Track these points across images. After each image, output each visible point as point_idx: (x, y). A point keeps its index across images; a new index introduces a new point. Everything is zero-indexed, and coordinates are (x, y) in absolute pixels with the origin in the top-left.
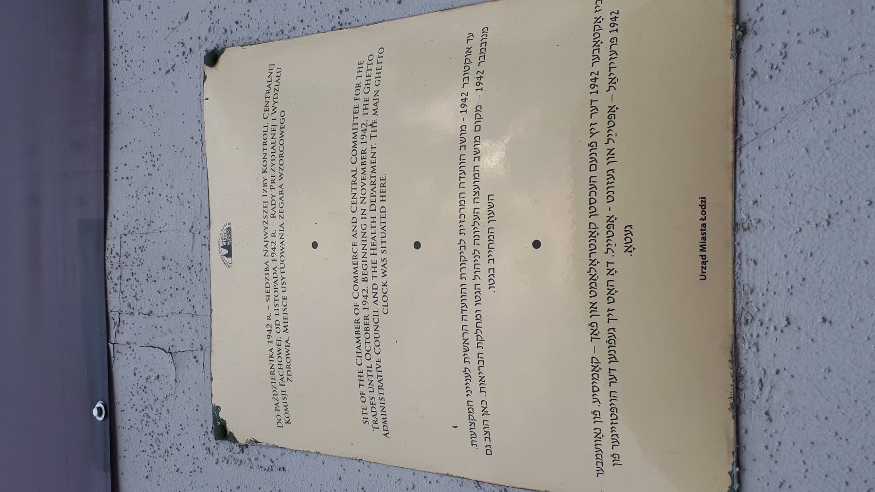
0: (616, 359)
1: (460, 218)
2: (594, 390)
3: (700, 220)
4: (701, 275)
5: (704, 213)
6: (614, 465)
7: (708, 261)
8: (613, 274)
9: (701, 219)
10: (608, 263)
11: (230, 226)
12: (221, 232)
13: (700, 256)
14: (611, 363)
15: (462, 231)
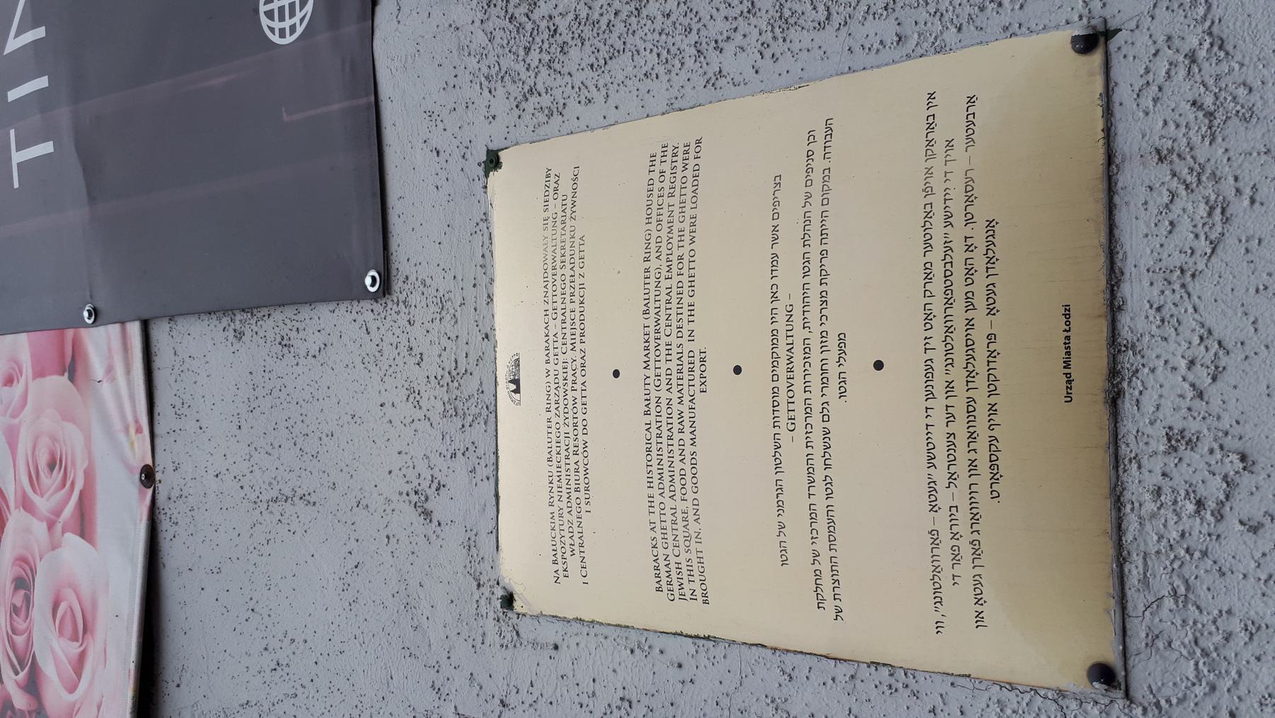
6: (977, 627)
9: (1065, 331)
10: (966, 238)
15: (809, 444)
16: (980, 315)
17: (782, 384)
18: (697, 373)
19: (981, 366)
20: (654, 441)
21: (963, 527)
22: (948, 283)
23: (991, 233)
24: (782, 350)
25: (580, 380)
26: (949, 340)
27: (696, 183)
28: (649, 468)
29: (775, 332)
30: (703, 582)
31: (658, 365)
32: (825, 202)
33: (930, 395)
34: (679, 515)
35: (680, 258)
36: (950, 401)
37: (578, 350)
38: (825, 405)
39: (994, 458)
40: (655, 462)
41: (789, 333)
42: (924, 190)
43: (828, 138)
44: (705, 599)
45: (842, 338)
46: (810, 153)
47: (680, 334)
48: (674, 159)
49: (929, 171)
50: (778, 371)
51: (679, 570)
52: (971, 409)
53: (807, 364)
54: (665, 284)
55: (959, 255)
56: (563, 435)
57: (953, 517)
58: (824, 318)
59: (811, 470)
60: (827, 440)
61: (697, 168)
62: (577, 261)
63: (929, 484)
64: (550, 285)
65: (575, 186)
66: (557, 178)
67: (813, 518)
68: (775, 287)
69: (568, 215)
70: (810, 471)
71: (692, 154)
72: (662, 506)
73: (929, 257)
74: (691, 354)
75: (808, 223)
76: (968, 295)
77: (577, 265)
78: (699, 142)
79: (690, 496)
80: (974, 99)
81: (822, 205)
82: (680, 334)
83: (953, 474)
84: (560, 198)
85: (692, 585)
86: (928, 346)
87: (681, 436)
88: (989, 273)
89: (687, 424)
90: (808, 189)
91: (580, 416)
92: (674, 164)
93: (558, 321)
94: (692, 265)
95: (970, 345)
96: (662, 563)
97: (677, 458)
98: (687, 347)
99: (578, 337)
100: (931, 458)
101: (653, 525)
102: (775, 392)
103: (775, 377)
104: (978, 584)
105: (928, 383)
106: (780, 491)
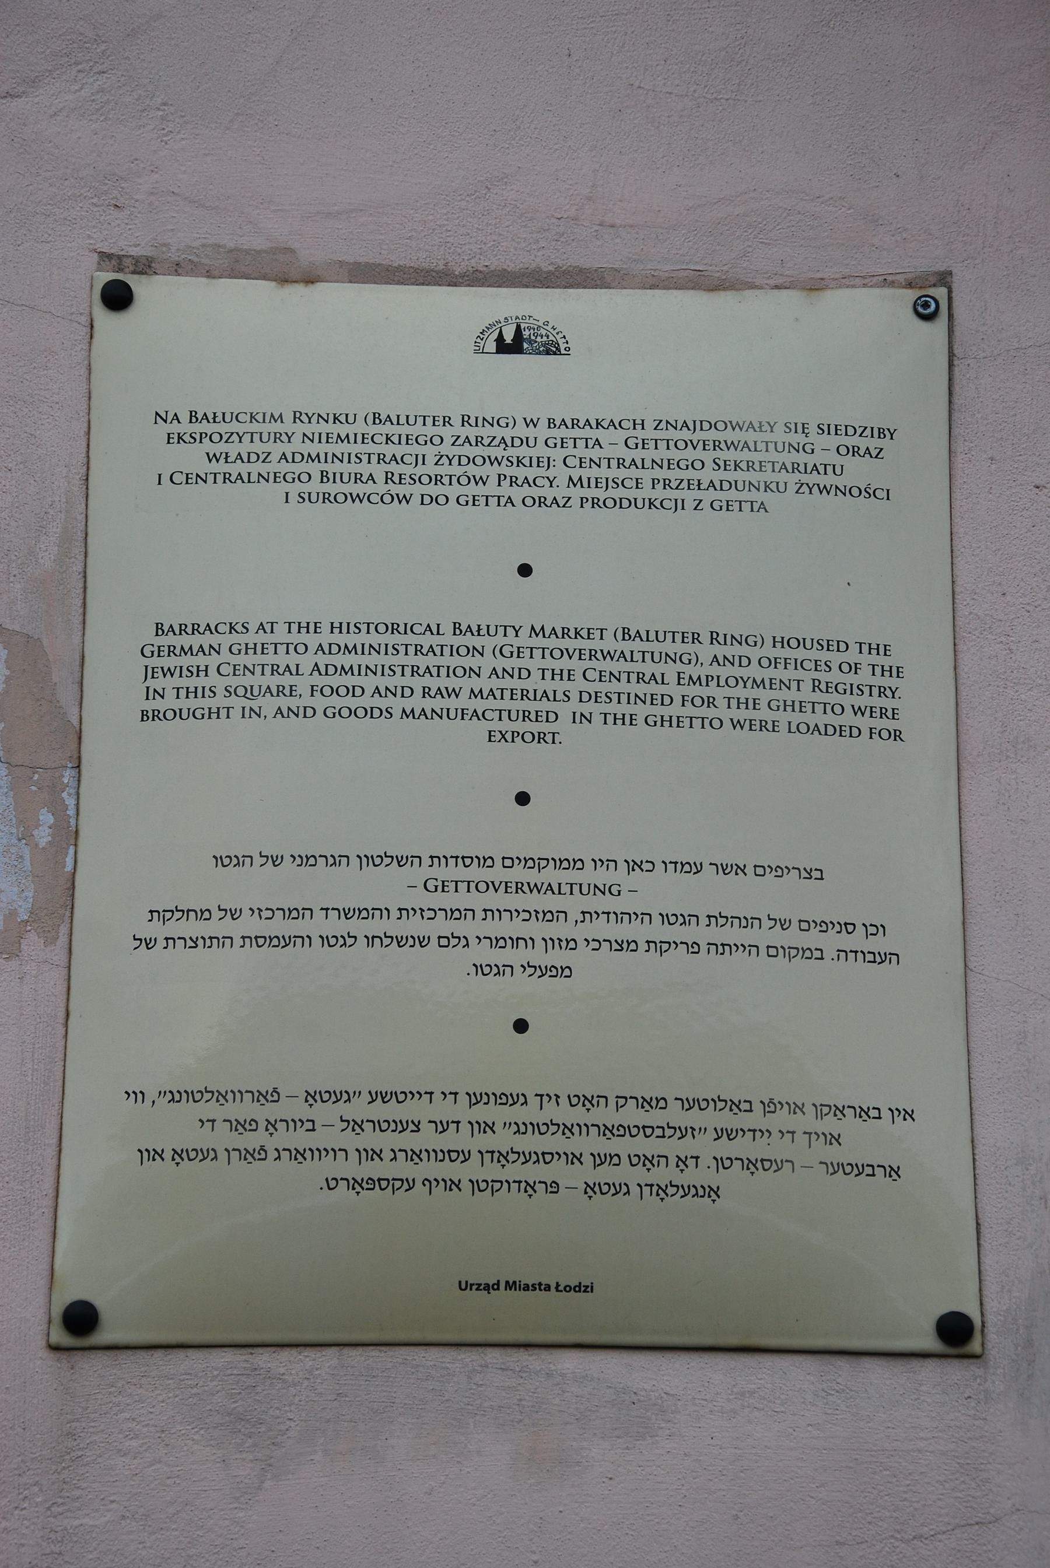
0: (599, 1165)
1: (429, 909)
2: (646, 1129)
3: (557, 1283)
4: (467, 1282)
5: (568, 1289)
6: (139, 1150)
7: (489, 1293)
8: (678, 1166)
9: (558, 1285)
10: (697, 1158)
11: (563, 352)
12: (550, 325)
13: (498, 1281)
14: (592, 1158)
16: (585, 1173)
17: (498, 874)
18: (520, 726)
19: (514, 1171)
20: (410, 639)
21: (284, 1138)
22: (634, 1131)
23: (701, 1192)
24: (551, 875)
25: (517, 493)
26: (553, 1129)
27: (830, 730)
28: (364, 628)
29: (579, 865)
30: (178, 714)
31: (538, 653)
32: (773, 951)
33: (475, 1099)
34: (287, 680)
35: (710, 702)
36: (465, 1127)
37: (568, 492)
38: (463, 942)
39: (384, 1184)
40: (374, 639)
41: (576, 888)
42: (771, 1101)
43: (870, 957)
44: (150, 714)
45: (564, 972)
46: (850, 928)
47: (585, 697)
48: (875, 691)
49: (797, 1108)
50: (518, 868)
51: (194, 670)
52: (454, 1155)
53: (526, 916)
54: (671, 670)
55: (673, 1147)
56: (420, 450)
57: (299, 1124)
58: (596, 945)
59: (364, 914)
60: (411, 941)
61: (855, 732)
62: (724, 496)
63: (346, 1092)
64: (686, 435)
65: (855, 492)
66: (874, 453)
67: (292, 913)
68: (650, 866)
69: (805, 478)
70: (363, 913)
71: (878, 723)
72: (301, 649)
73: (675, 1106)
74: (552, 717)
75: (744, 923)
76: (616, 1158)
77: (719, 495)
78: (896, 735)
79: (319, 702)
80: (895, 1176)
81: (768, 947)
82: (585, 697)
83: (360, 1127)
84: (838, 460)
85: (170, 694)
86: (546, 1099)
87: (418, 692)
88: (512, 1185)
89: (438, 703)
90: (795, 924)
91: (454, 491)
92: (866, 690)
93: (621, 452)
94: (697, 723)
95: (544, 1157)
96: (207, 640)
97: (382, 682)
98: (565, 710)
99: (592, 493)
100: (384, 1097)
101: (268, 628)
102: (486, 861)
103: (508, 863)
104: (205, 1154)
105: (492, 1098)
106: (331, 861)
